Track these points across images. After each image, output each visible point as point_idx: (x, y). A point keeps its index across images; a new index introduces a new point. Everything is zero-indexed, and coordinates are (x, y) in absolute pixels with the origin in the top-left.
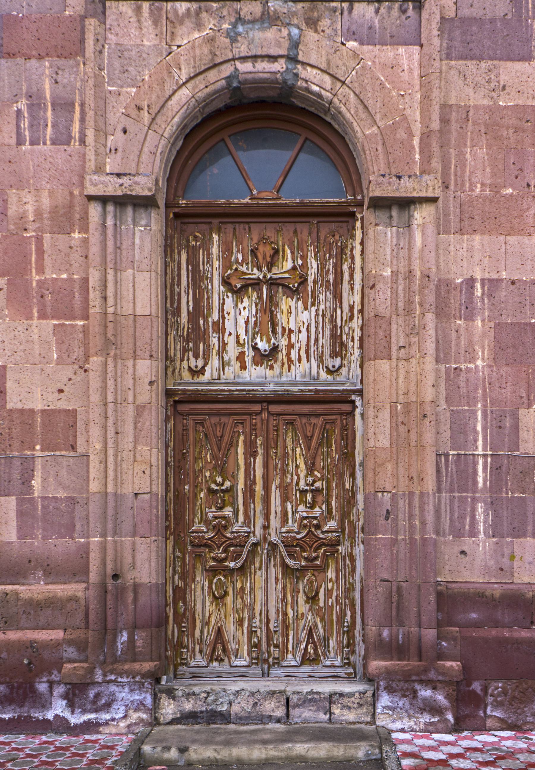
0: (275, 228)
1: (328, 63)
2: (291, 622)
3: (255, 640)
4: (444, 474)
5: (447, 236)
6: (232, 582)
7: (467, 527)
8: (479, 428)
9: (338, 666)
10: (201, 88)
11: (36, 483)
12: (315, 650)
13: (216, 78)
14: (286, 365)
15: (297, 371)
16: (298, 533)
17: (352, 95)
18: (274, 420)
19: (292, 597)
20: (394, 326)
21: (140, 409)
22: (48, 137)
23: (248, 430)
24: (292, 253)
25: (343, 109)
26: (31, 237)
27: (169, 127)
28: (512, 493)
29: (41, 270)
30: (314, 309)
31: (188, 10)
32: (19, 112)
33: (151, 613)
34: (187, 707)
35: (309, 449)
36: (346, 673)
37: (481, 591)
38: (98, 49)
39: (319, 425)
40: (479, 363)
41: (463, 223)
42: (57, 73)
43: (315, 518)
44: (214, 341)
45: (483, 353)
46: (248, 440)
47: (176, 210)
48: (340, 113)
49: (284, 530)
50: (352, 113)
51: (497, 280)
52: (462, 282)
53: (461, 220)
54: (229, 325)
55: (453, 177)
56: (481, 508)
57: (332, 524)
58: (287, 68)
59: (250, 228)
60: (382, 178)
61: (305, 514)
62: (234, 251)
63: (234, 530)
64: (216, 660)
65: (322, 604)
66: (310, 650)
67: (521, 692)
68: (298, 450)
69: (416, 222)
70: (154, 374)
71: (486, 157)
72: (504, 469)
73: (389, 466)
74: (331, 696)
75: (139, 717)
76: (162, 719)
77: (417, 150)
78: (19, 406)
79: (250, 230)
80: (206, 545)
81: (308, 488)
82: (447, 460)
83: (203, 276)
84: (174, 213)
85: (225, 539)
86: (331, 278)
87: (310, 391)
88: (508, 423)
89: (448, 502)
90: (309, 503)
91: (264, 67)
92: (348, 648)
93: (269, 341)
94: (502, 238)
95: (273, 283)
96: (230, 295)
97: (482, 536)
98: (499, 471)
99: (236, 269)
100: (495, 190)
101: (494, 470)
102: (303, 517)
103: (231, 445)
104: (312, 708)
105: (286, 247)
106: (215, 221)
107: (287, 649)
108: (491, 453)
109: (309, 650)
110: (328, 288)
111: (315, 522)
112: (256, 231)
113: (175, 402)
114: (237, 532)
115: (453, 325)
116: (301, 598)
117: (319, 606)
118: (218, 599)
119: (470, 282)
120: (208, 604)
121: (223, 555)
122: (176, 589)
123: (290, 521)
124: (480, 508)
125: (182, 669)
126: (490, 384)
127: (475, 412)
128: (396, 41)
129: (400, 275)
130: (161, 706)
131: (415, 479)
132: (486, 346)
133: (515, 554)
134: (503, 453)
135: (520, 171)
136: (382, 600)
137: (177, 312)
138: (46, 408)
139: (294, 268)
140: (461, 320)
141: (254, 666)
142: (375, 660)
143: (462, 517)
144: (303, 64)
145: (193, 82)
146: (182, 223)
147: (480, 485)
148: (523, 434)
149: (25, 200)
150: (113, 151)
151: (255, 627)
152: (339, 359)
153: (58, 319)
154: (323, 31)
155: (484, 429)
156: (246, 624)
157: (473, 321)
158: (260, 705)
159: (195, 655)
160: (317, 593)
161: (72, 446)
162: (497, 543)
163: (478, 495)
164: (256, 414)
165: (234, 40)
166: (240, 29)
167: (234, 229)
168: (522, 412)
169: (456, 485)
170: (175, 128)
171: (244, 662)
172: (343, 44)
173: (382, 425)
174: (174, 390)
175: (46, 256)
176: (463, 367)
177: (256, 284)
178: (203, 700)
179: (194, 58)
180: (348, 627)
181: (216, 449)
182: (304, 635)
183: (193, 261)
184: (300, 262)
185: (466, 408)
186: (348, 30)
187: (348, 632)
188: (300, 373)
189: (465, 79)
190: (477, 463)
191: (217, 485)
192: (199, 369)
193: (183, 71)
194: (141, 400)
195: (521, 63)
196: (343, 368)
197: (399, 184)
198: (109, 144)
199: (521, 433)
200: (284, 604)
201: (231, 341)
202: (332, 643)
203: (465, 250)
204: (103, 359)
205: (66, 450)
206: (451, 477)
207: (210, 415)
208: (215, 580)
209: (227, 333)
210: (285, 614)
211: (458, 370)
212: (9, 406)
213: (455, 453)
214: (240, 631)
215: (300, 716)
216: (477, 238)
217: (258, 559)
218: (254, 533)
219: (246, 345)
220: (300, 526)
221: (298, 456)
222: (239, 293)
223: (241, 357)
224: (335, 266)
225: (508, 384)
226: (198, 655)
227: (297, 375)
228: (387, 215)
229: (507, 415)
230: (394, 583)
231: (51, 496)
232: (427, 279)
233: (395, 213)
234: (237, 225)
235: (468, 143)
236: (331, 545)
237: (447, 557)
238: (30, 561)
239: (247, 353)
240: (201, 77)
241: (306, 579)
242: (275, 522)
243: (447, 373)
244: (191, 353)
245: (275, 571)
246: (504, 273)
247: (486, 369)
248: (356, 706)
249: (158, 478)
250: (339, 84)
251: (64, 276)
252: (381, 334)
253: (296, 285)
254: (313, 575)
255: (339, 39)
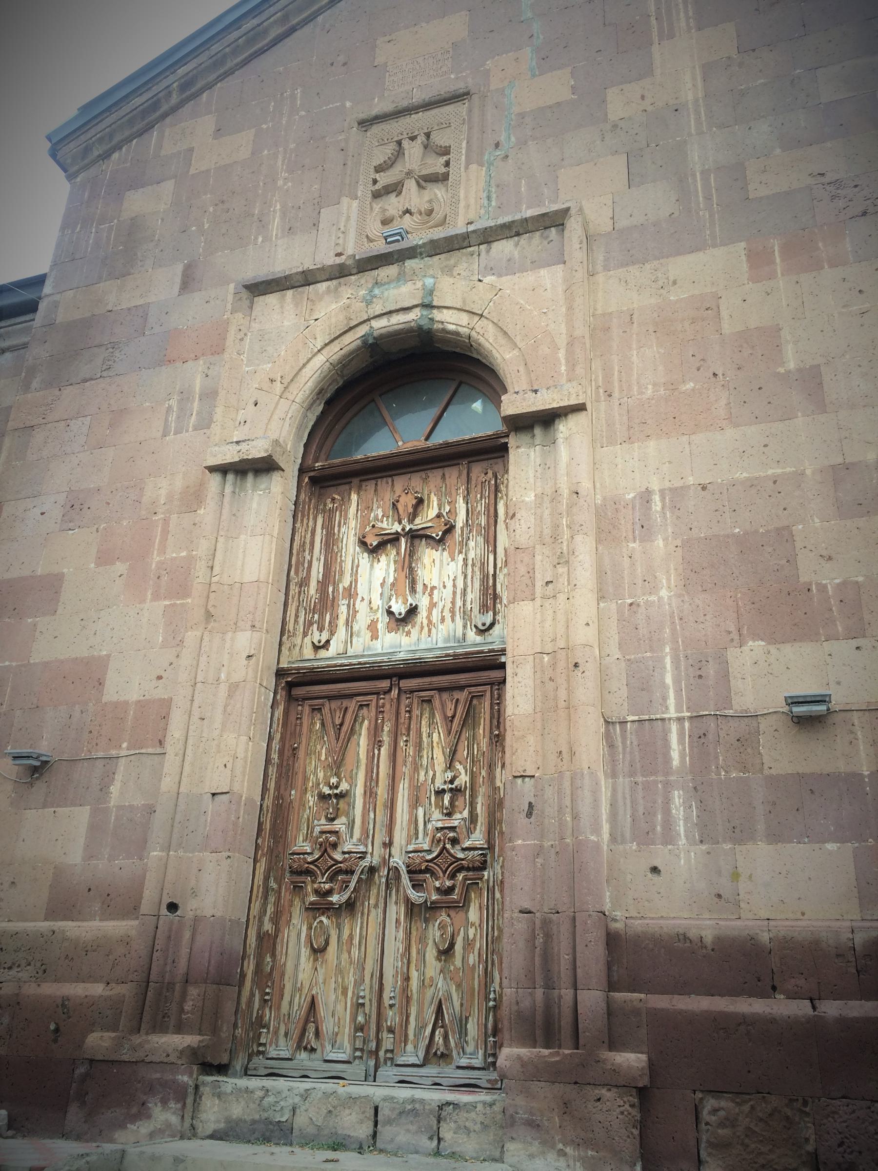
0: (421, 477)
1: (464, 302)
2: (415, 991)
3: (360, 1019)
4: (620, 749)
5: (612, 448)
6: (339, 927)
7: (659, 828)
8: (669, 680)
9: (479, 1069)
10: (335, 352)
11: (115, 789)
12: (446, 1037)
13: (352, 340)
14: (426, 629)
15: (440, 635)
16: (429, 851)
17: (491, 325)
18: (407, 698)
19: (418, 953)
20: (538, 558)
21: (233, 688)
22: (191, 425)
23: (373, 713)
24: (439, 500)
25: (482, 340)
26: (159, 519)
27: (302, 392)
28: (726, 772)
29: (163, 550)
30: (461, 557)
31: (328, 287)
32: (170, 408)
33: (209, 962)
34: (236, 1112)
35: (450, 733)
36: (489, 1081)
37: (681, 931)
38: (239, 337)
39: (462, 701)
40: (664, 593)
41: (632, 431)
42: (209, 368)
43: (453, 829)
44: (343, 610)
45: (669, 580)
46: (373, 726)
47: (312, 474)
48: (480, 345)
49: (411, 848)
50: (491, 341)
51: (682, 487)
52: (635, 497)
53: (630, 428)
54: (362, 589)
55: (616, 384)
56: (679, 798)
57: (478, 838)
58: (422, 315)
59: (393, 481)
60: (515, 395)
61: (440, 825)
62: (374, 508)
63: (346, 850)
64: (305, 1048)
65: (458, 962)
66: (438, 1038)
67: (761, 1120)
68: (435, 735)
69: (561, 435)
70: (253, 646)
71: (657, 356)
72: (710, 737)
73: (531, 739)
74: (440, 1108)
75: (167, 1120)
76: (200, 1130)
77: (563, 361)
78: (115, 698)
79: (393, 484)
80: (308, 872)
81: (445, 787)
82: (624, 731)
83: (338, 539)
84: (309, 477)
85: (333, 862)
86: (483, 521)
87: (447, 655)
88: (711, 670)
89: (627, 791)
90: (447, 808)
91: (398, 321)
92: (494, 1037)
93: (405, 601)
94: (685, 438)
95: (415, 536)
96: (366, 555)
97: (683, 841)
98: (702, 740)
99: (373, 526)
100: (673, 387)
101: (695, 739)
102: (437, 829)
103: (352, 731)
104: (411, 1127)
105: (432, 495)
106: (356, 481)
107: (406, 1036)
108: (689, 714)
109: (437, 1039)
110: (479, 533)
111: (451, 835)
112: (400, 483)
113: (290, 686)
114: (349, 853)
115: (624, 550)
116: (431, 953)
117: (455, 966)
118: (318, 951)
119: (646, 497)
120: (303, 959)
121: (327, 886)
122: (262, 937)
123: (421, 835)
124: (677, 797)
125: (259, 1061)
126: (681, 619)
127: (661, 660)
128: (536, 265)
129: (546, 498)
130: (202, 1108)
131: (565, 755)
132: (672, 571)
133: (740, 870)
134: (707, 713)
135: (702, 362)
136: (521, 944)
137: (304, 583)
138: (142, 698)
139: (439, 516)
140: (635, 542)
141: (357, 1062)
142: (510, 1046)
143: (649, 814)
144: (438, 307)
145: (328, 347)
146: (321, 488)
147: (676, 761)
148: (736, 684)
149: (160, 486)
150: (242, 423)
151: (363, 997)
152: (491, 613)
153: (171, 599)
154: (459, 274)
155: (677, 681)
156: (350, 994)
157: (653, 541)
158: (336, 1116)
159: (277, 1040)
160: (452, 945)
161: (160, 741)
162: (708, 853)
163: (672, 778)
164: (385, 693)
165: (369, 303)
166: (376, 291)
167: (376, 484)
168: (732, 654)
169: (638, 765)
170: (307, 392)
171: (343, 1055)
172: (480, 281)
173: (523, 684)
174: (288, 669)
175: (170, 536)
176: (641, 601)
177: (394, 539)
178: (257, 1102)
179: (330, 327)
180: (495, 1000)
181: (334, 741)
182: (430, 1015)
183: (329, 528)
184: (447, 508)
185: (648, 654)
186: (485, 268)
187: (495, 1007)
188: (438, 635)
189: (627, 285)
190: (670, 731)
191: (331, 788)
192: (321, 644)
193: (318, 340)
194: (237, 677)
195: (694, 254)
196: (497, 627)
197: (535, 398)
198: (239, 419)
199: (733, 682)
200: (405, 961)
201: (361, 607)
202: (472, 1028)
203: (636, 459)
204: (199, 634)
205: (153, 747)
206: (631, 753)
207: (330, 698)
208: (315, 924)
209: (359, 598)
210: (407, 979)
211: (634, 606)
212: (105, 699)
213: (636, 718)
214: (343, 1004)
215: (392, 1140)
216: (652, 443)
217: (374, 892)
218: (372, 854)
219: (380, 610)
220: (433, 841)
221: (435, 744)
222: (374, 551)
223: (372, 627)
224: (487, 507)
225: (707, 617)
226: (282, 1041)
227: (439, 640)
228: (530, 436)
229: (710, 659)
230: (538, 914)
231: (127, 804)
232: (575, 496)
233: (538, 431)
234: (379, 480)
235: (634, 346)
236: (474, 869)
237: (629, 877)
238: (90, 890)
239: (380, 620)
240: (337, 341)
241: (438, 922)
242: (400, 837)
243: (620, 611)
244: (315, 626)
245: (396, 911)
246: (691, 478)
247: (674, 600)
248: (478, 1127)
249: (243, 773)
250: (477, 318)
251: (184, 554)
252: (522, 570)
253: (440, 533)
254: (449, 916)
255: (476, 278)
